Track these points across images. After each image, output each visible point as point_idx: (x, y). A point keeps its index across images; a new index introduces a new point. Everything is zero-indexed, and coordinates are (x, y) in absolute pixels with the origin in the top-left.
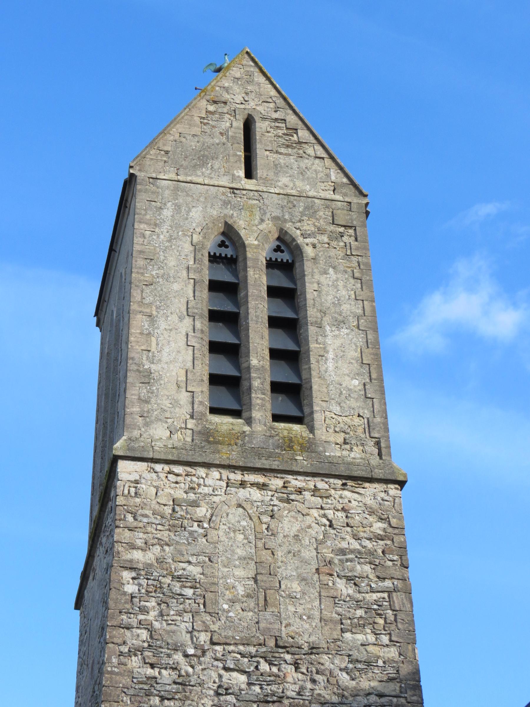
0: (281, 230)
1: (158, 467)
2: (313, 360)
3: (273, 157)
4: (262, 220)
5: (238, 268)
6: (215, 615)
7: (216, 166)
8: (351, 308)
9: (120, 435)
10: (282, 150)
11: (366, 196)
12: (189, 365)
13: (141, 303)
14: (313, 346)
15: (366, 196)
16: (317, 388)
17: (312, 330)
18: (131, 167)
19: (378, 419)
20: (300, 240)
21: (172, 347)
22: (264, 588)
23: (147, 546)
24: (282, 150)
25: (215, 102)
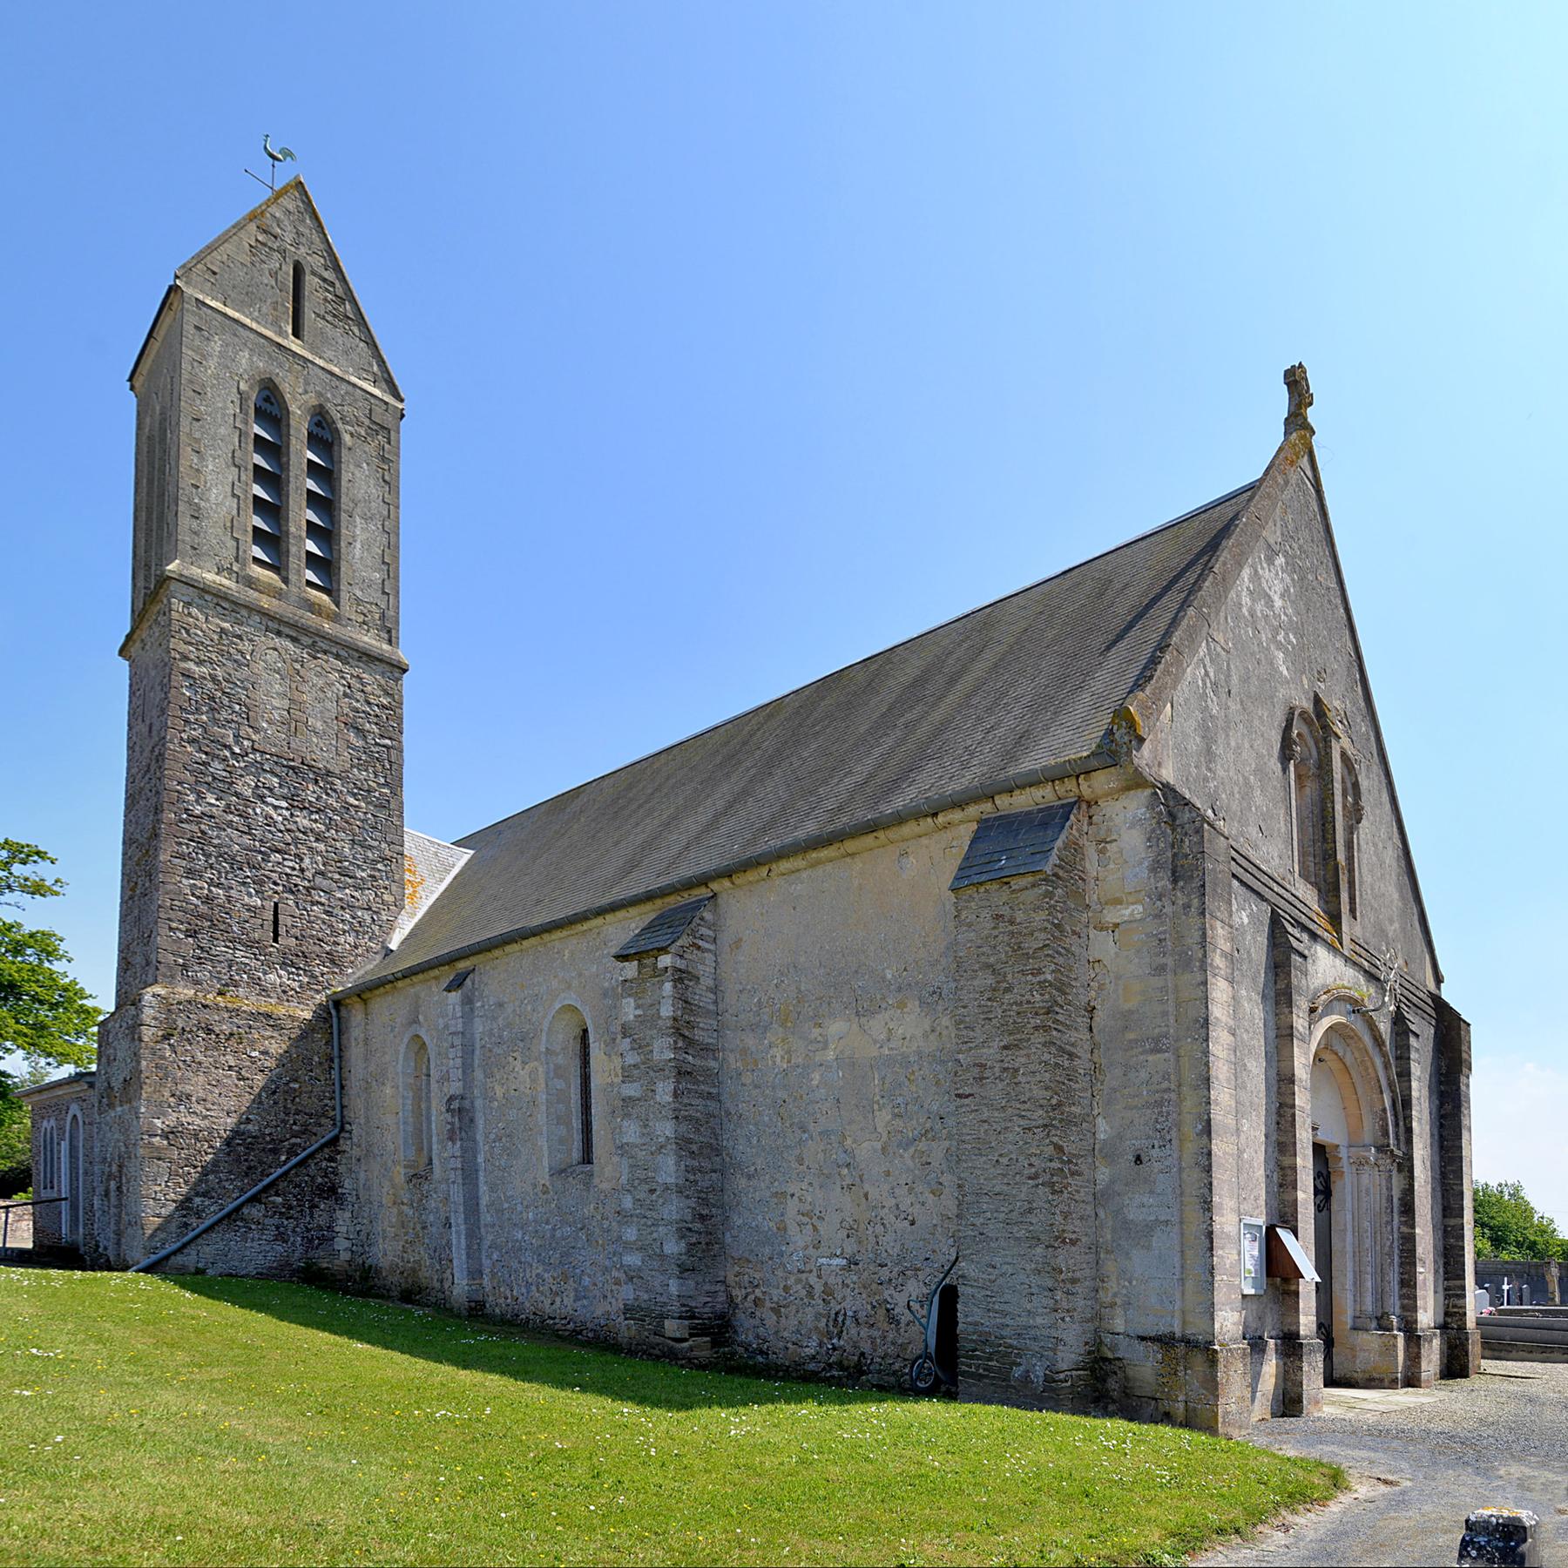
0: (321, 406)
1: (208, 597)
2: (343, 544)
3: (321, 323)
4: (306, 392)
5: (355, 1053)
6: (256, 730)
7: (264, 310)
8: (377, 506)
9: (527, 1373)
10: (329, 318)
11: (402, 401)
12: (235, 512)
13: (190, 435)
14: (343, 531)
15: (402, 401)
16: (345, 502)
17: (344, 516)
18: (177, 277)
19: (392, 613)
20: (340, 425)
21: (218, 486)
22: (293, 723)
23: (200, 663)
24: (329, 318)
25: (265, 232)
